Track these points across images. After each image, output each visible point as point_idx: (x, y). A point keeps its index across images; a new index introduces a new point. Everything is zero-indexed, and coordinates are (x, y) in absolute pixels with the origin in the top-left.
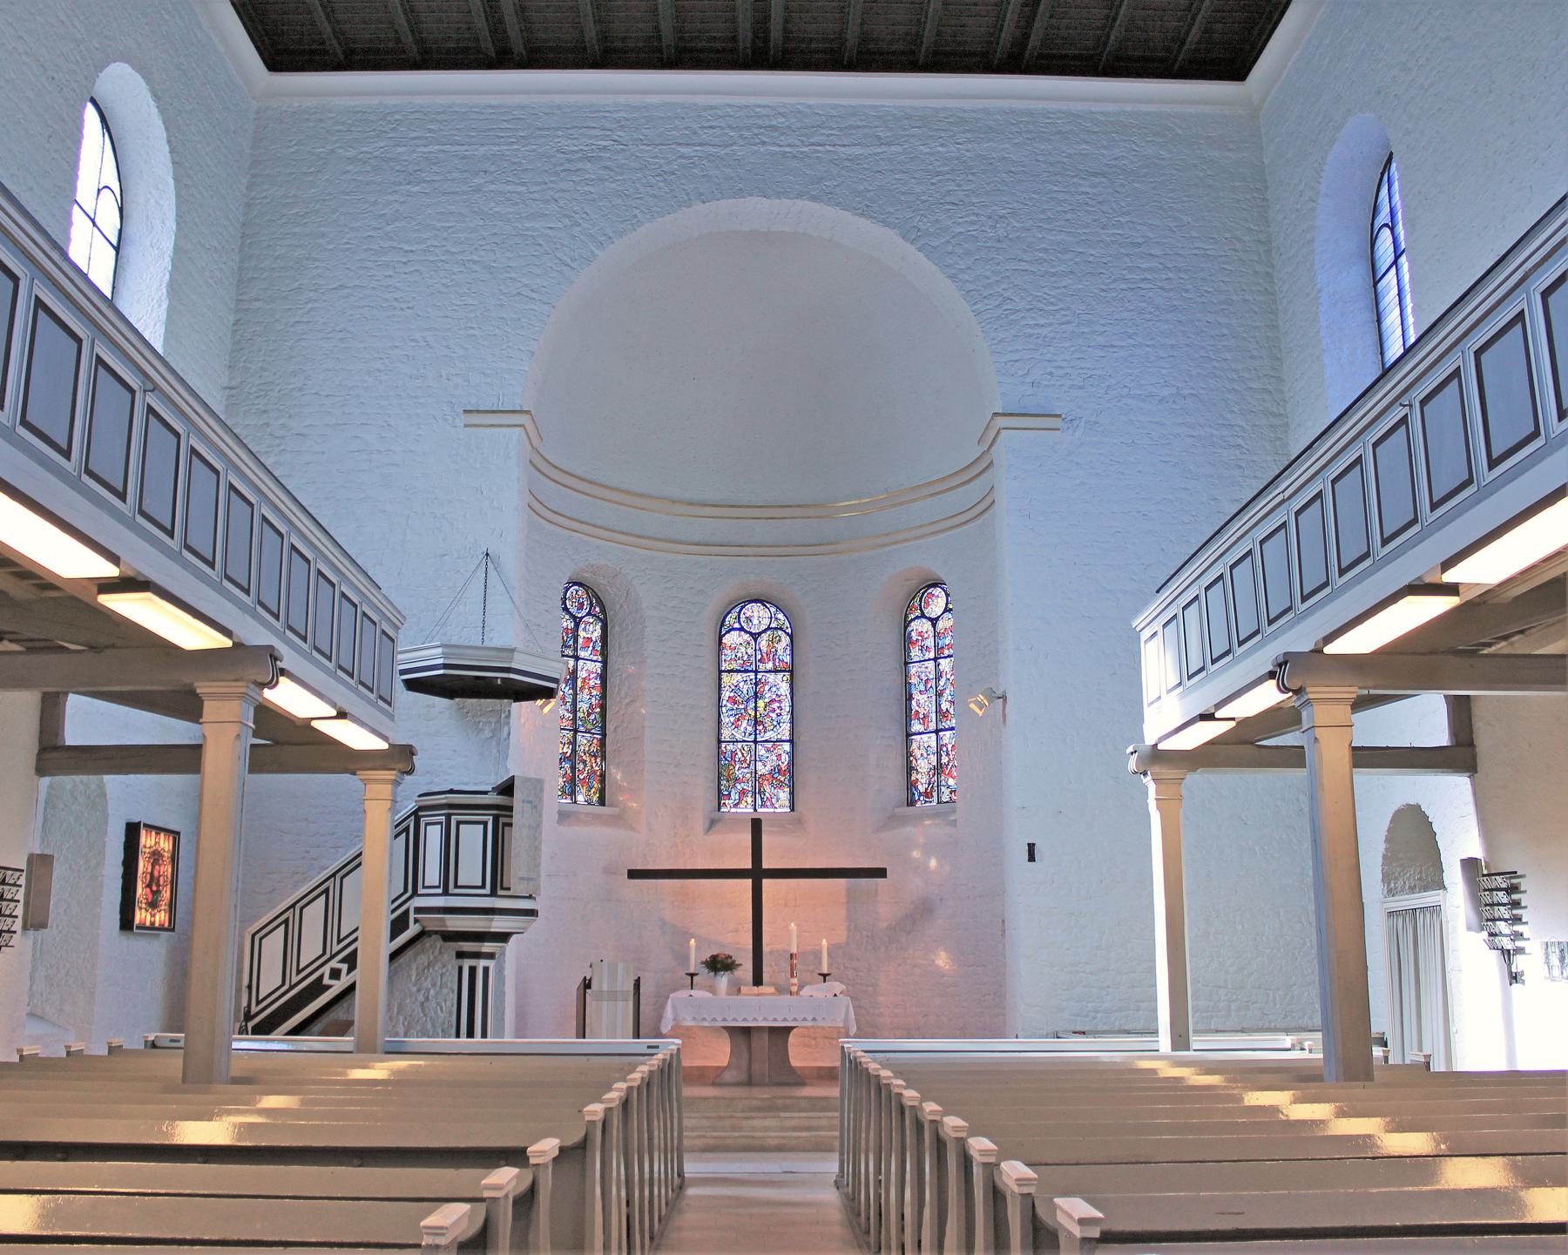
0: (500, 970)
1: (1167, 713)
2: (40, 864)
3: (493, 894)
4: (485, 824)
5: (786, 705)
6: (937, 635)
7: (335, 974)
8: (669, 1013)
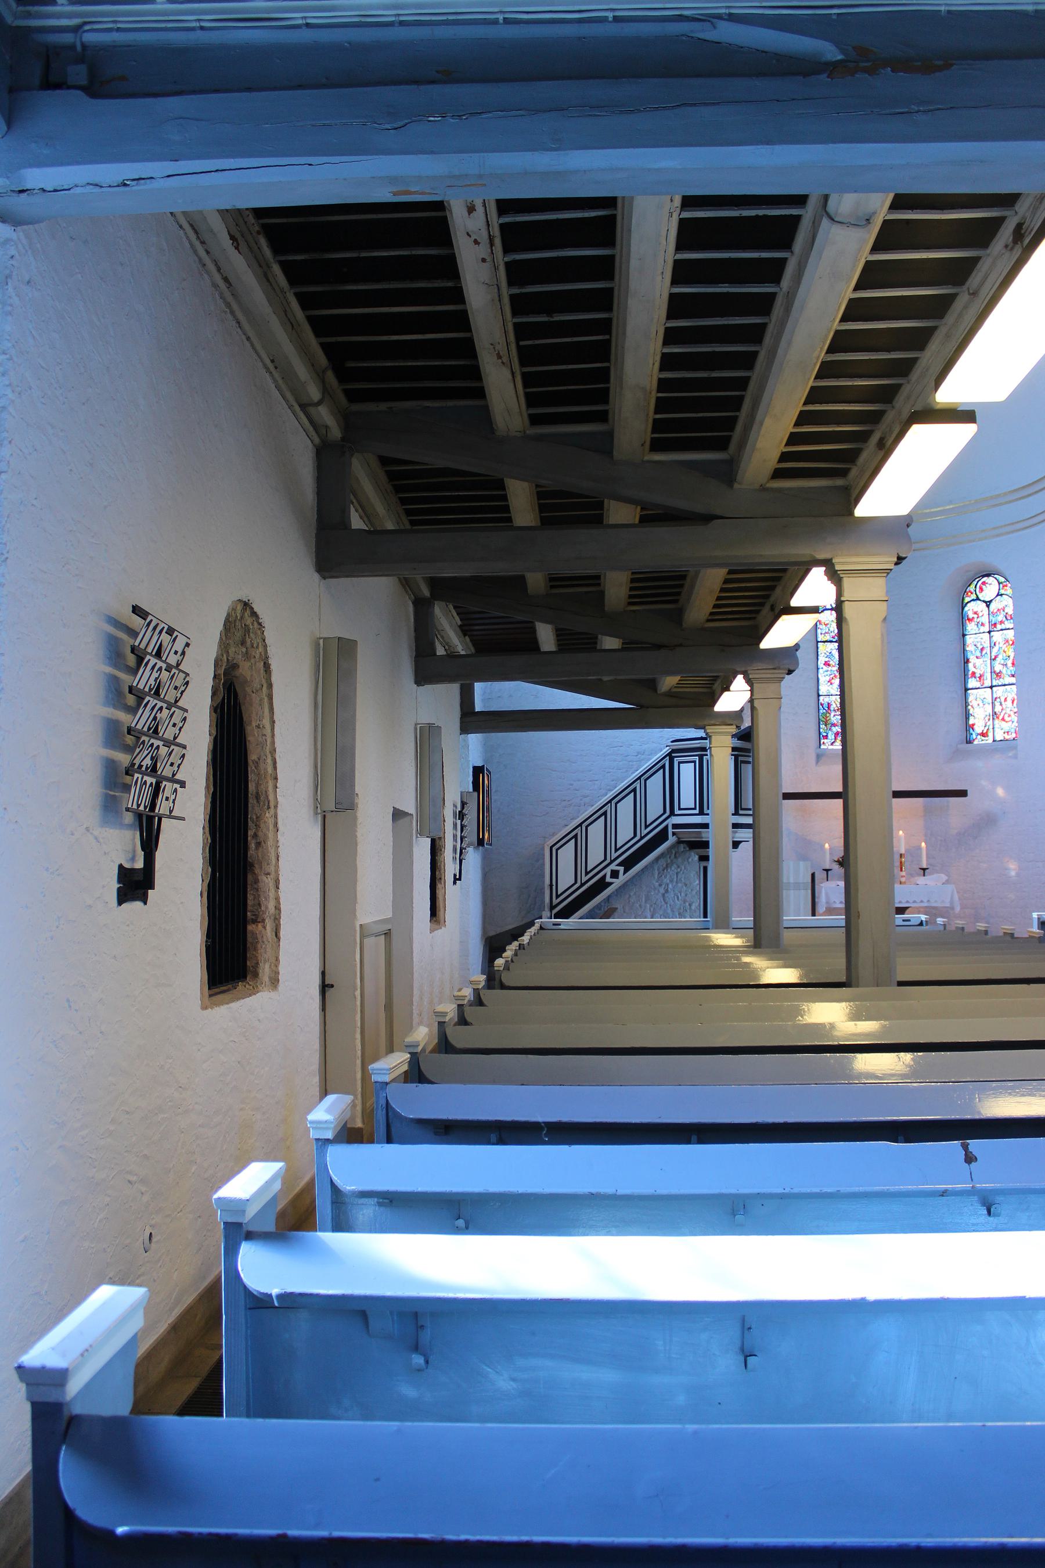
4: (694, 762)
7: (615, 874)
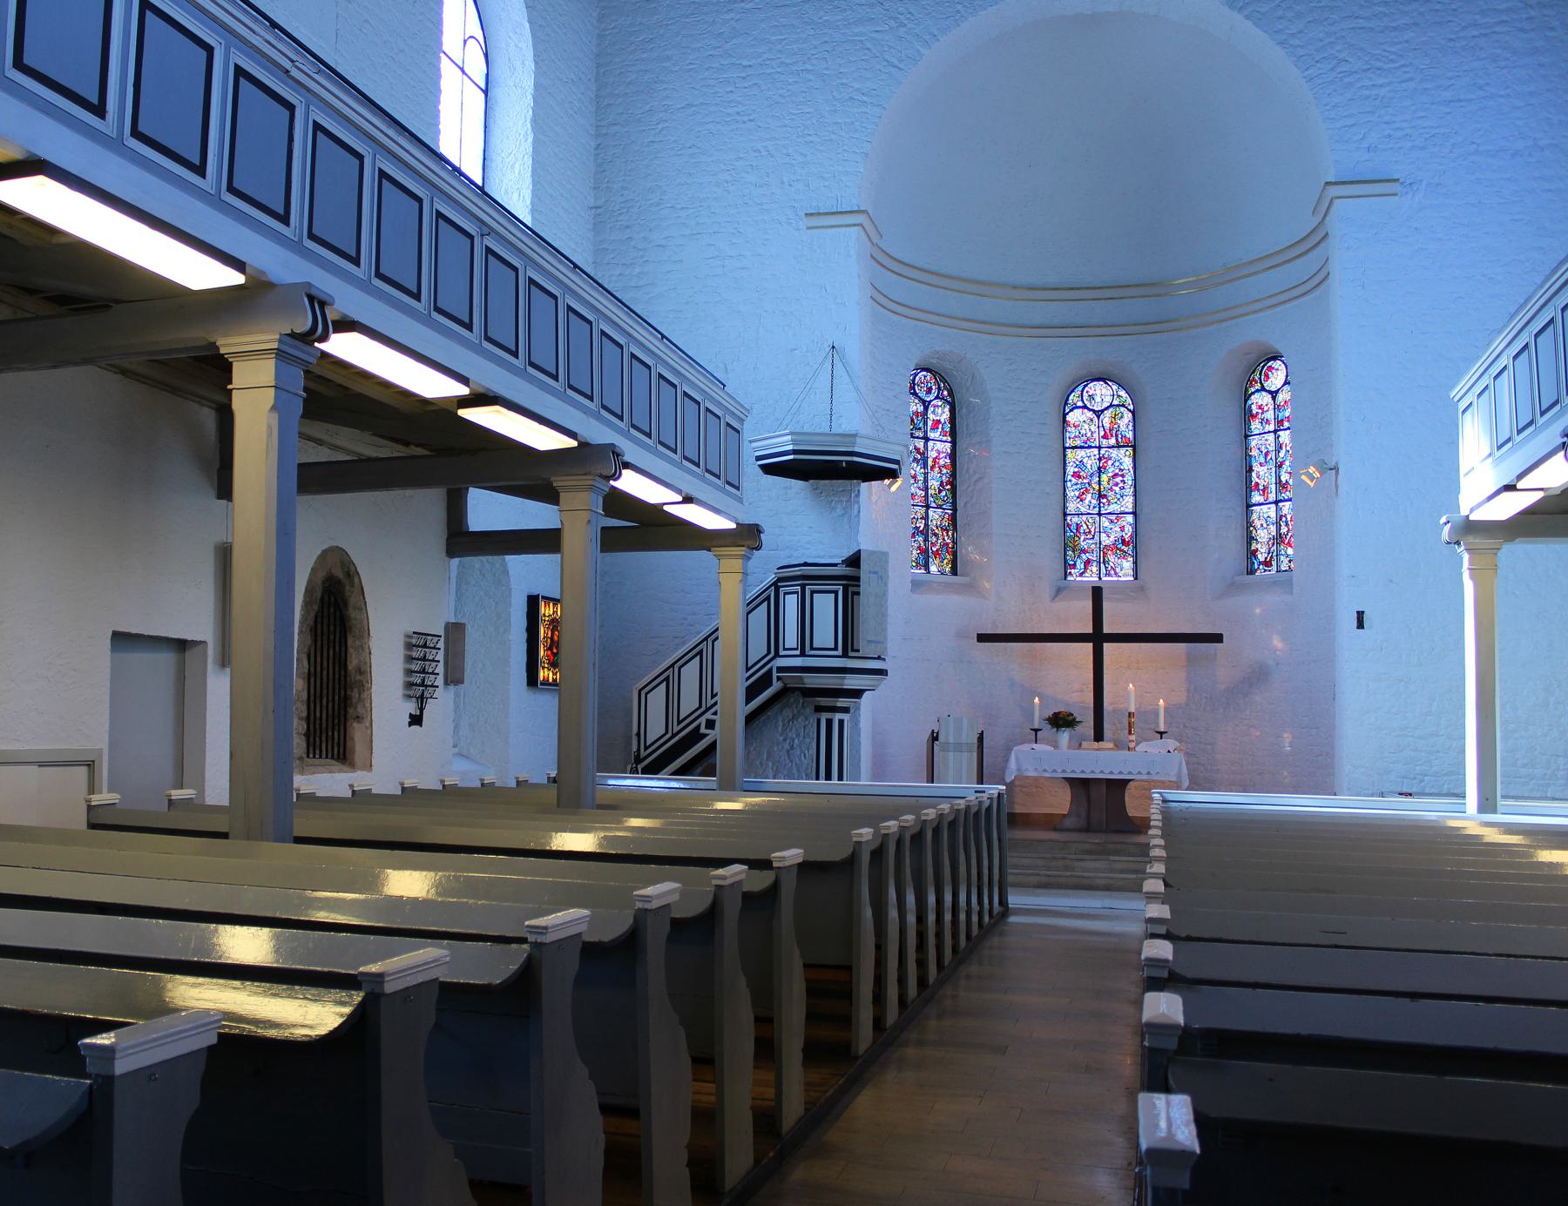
0: (856, 723)
1: (1484, 484)
2: (455, 631)
3: (845, 655)
4: (836, 593)
5: (1129, 479)
6: (1277, 408)
8: (1012, 764)
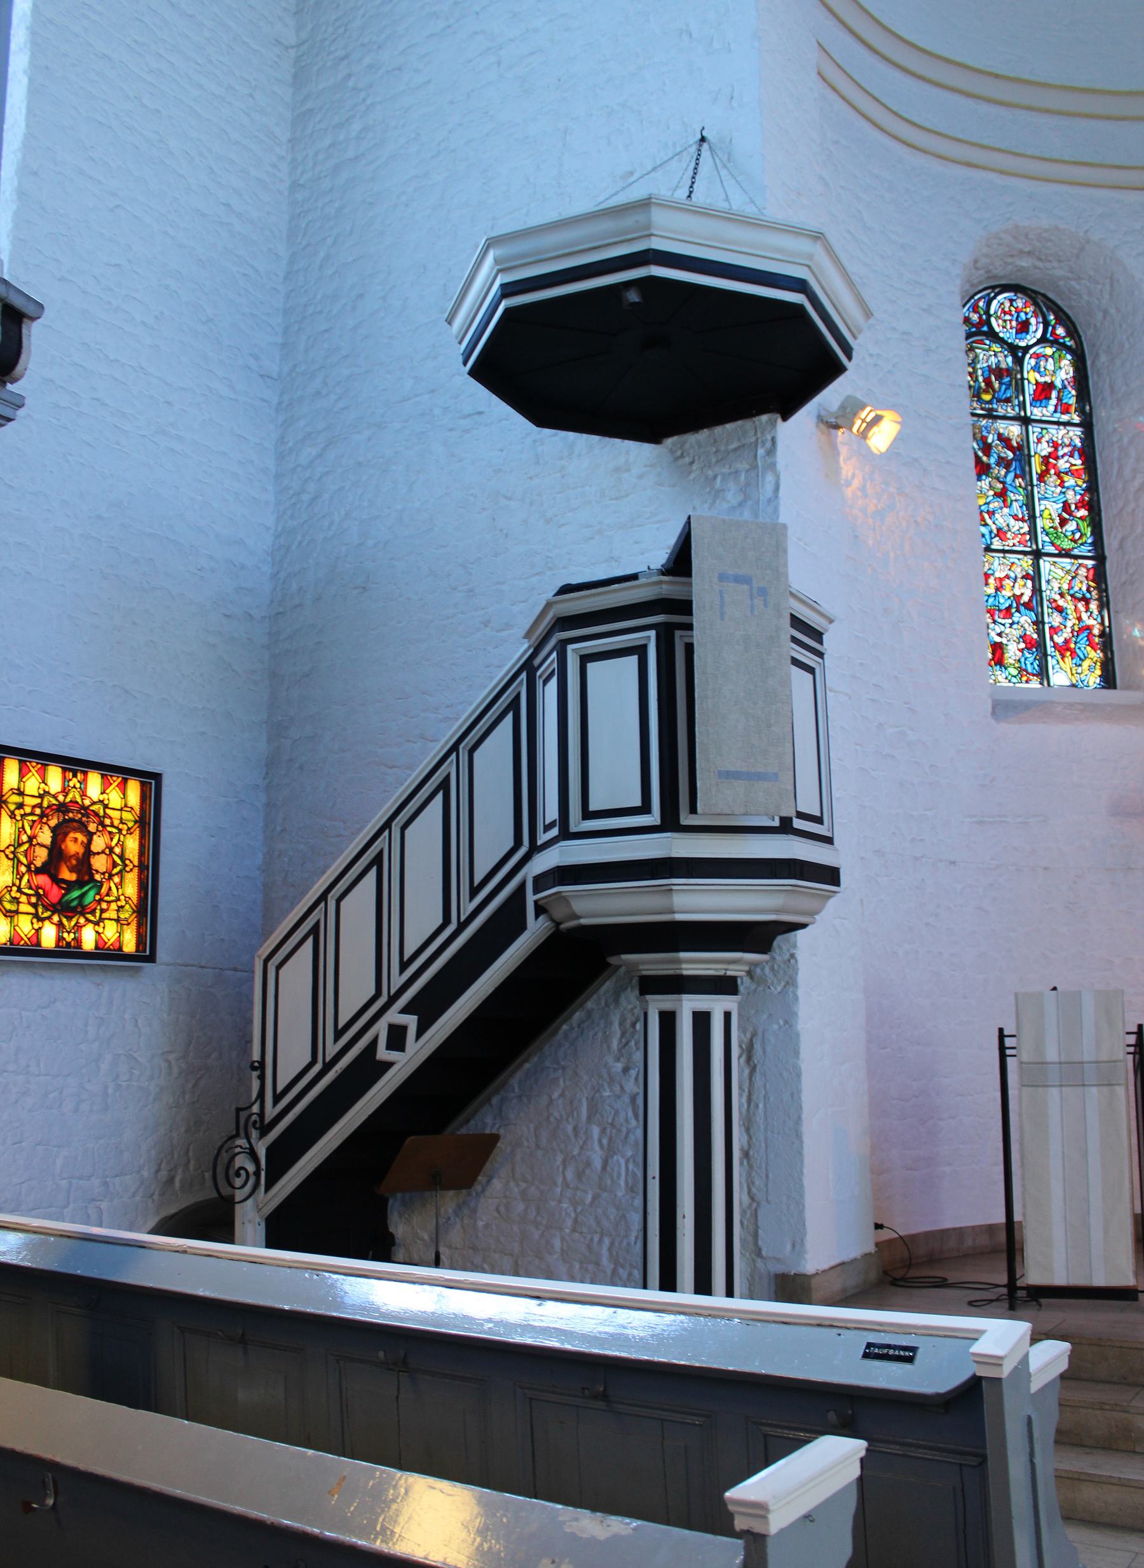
3: (670, 823)
4: (640, 651)
